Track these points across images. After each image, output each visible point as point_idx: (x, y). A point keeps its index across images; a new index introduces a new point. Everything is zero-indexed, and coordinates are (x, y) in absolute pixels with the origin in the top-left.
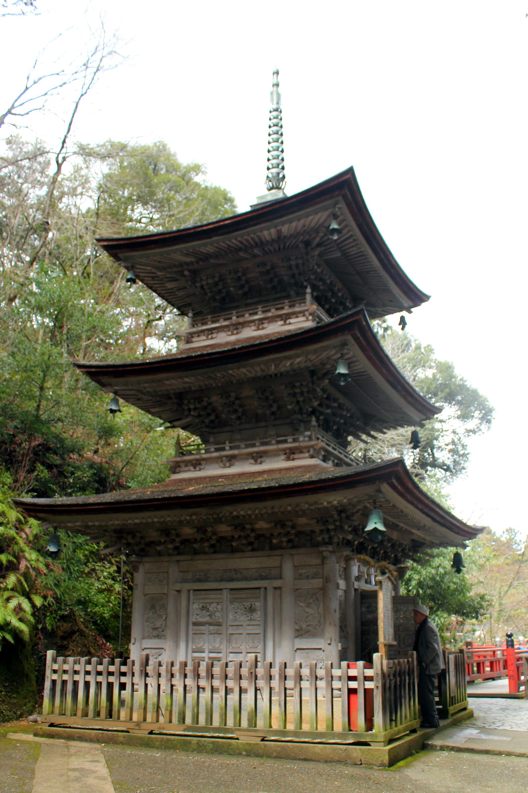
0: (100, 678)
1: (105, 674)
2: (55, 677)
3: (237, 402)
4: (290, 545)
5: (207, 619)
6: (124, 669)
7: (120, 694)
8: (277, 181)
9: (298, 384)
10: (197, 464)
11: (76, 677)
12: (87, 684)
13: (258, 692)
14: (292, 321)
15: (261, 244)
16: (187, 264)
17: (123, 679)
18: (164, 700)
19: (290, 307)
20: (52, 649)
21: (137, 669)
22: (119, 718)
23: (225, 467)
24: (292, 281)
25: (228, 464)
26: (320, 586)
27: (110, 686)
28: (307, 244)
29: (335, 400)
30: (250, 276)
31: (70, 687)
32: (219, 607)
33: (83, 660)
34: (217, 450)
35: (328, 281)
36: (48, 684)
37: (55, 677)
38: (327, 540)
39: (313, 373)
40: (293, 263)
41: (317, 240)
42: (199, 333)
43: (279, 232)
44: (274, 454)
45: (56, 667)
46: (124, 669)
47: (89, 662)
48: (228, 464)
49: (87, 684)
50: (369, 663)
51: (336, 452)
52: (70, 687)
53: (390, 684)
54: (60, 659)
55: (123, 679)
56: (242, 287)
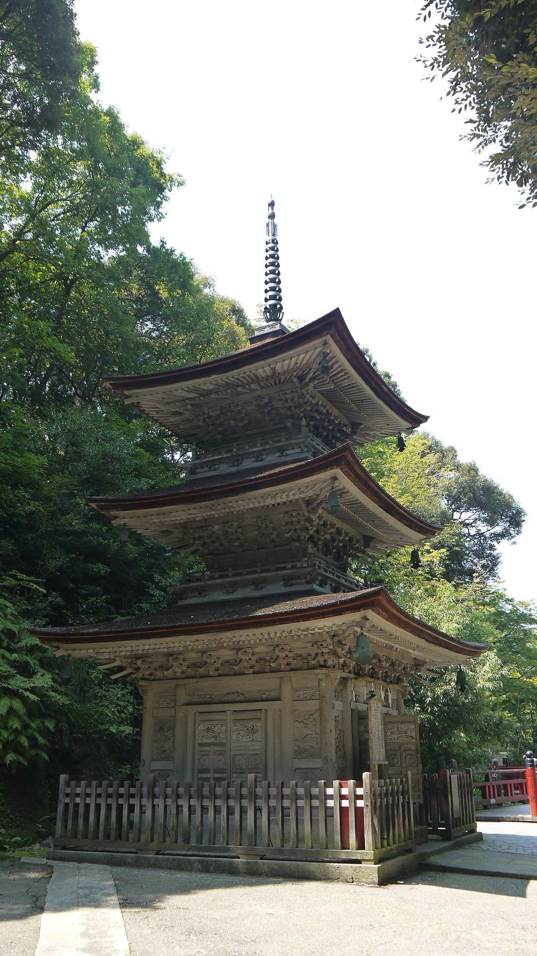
0: (110, 801)
1: (115, 797)
2: (67, 800)
3: (240, 530)
4: (289, 668)
5: (212, 740)
6: (132, 791)
7: (129, 816)
8: (274, 311)
9: (295, 513)
10: (201, 591)
11: (88, 801)
12: (98, 807)
13: (258, 812)
14: (288, 452)
15: (257, 380)
16: (189, 399)
17: (132, 801)
18: (172, 821)
19: (287, 439)
20: (65, 773)
21: (145, 790)
22: (128, 839)
23: (228, 593)
24: (289, 413)
25: (231, 590)
26: (317, 707)
27: (120, 808)
28: (301, 378)
29: (333, 526)
30: (248, 409)
31: (81, 809)
32: (223, 729)
33: (94, 783)
34: (221, 577)
35: (324, 411)
36: (60, 808)
37: (67, 800)
38: (322, 663)
39: (308, 502)
40: (289, 396)
41: (311, 375)
42: (202, 465)
43: (274, 369)
44: (273, 581)
45: (68, 790)
46: (132, 791)
47: (100, 785)
48: (231, 590)
49: (98, 807)
50: (359, 784)
51: (334, 577)
52: (81, 809)
53: (381, 802)
54: (73, 783)
55: (132, 801)
56: (242, 419)
